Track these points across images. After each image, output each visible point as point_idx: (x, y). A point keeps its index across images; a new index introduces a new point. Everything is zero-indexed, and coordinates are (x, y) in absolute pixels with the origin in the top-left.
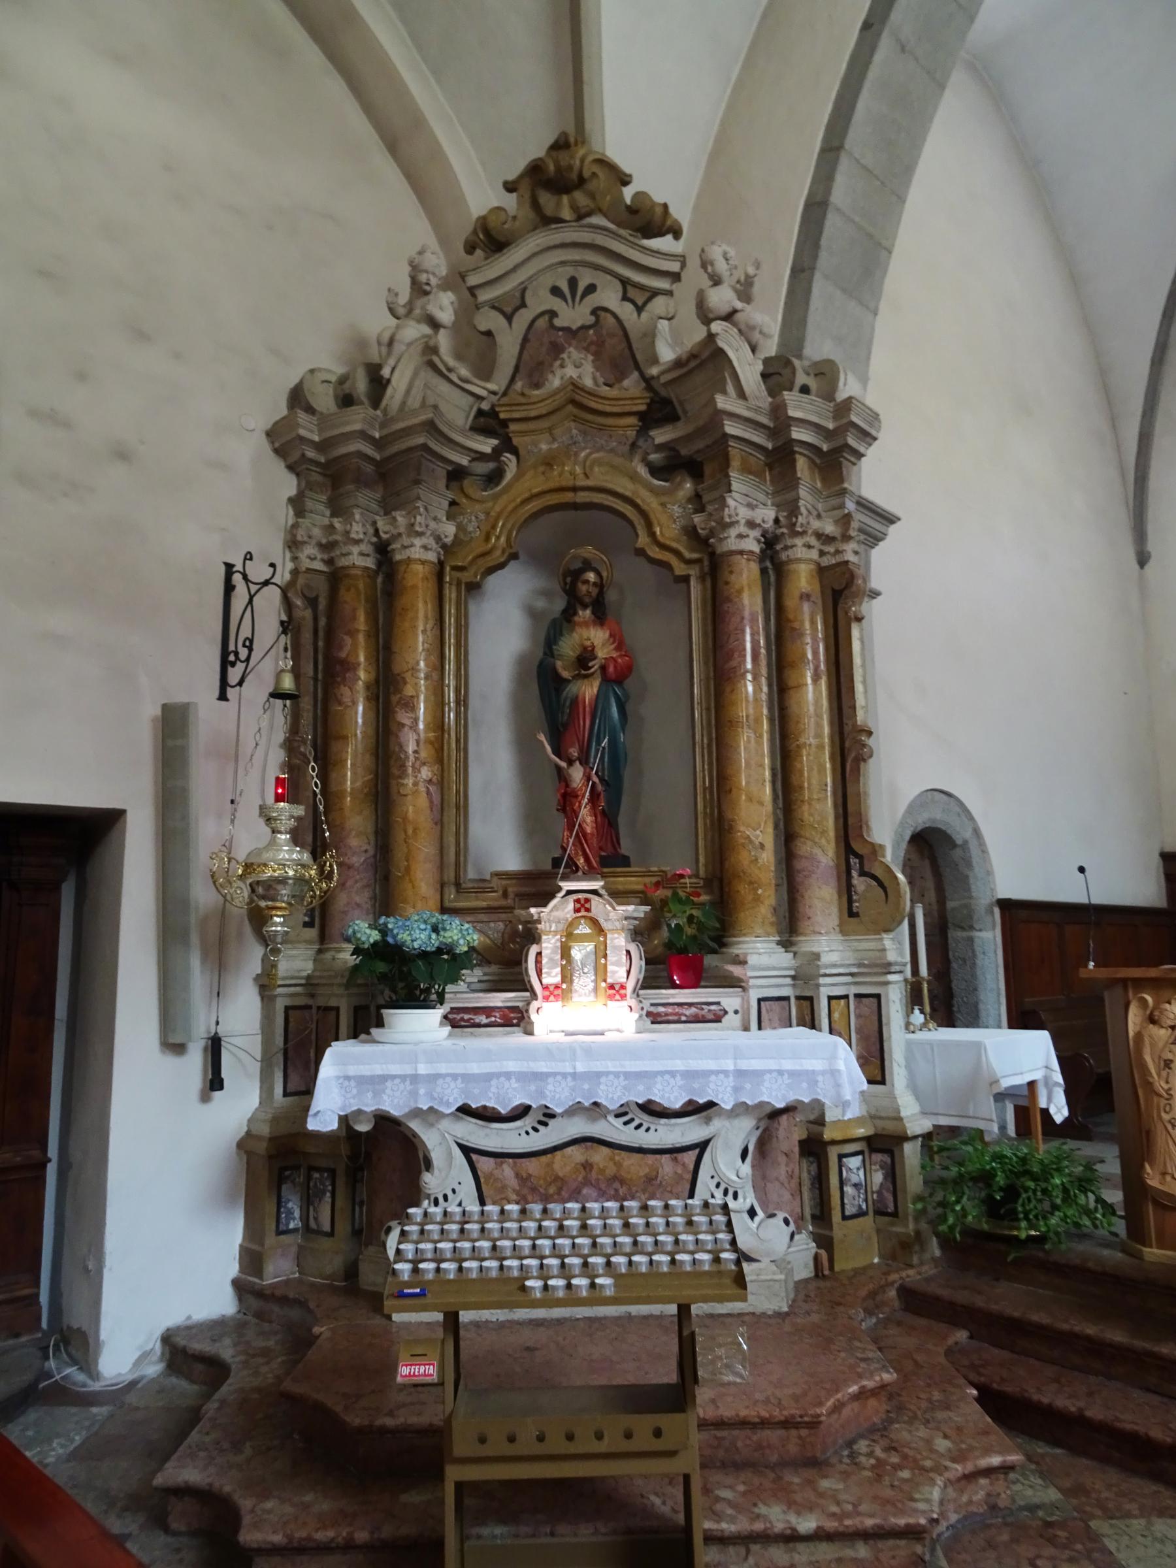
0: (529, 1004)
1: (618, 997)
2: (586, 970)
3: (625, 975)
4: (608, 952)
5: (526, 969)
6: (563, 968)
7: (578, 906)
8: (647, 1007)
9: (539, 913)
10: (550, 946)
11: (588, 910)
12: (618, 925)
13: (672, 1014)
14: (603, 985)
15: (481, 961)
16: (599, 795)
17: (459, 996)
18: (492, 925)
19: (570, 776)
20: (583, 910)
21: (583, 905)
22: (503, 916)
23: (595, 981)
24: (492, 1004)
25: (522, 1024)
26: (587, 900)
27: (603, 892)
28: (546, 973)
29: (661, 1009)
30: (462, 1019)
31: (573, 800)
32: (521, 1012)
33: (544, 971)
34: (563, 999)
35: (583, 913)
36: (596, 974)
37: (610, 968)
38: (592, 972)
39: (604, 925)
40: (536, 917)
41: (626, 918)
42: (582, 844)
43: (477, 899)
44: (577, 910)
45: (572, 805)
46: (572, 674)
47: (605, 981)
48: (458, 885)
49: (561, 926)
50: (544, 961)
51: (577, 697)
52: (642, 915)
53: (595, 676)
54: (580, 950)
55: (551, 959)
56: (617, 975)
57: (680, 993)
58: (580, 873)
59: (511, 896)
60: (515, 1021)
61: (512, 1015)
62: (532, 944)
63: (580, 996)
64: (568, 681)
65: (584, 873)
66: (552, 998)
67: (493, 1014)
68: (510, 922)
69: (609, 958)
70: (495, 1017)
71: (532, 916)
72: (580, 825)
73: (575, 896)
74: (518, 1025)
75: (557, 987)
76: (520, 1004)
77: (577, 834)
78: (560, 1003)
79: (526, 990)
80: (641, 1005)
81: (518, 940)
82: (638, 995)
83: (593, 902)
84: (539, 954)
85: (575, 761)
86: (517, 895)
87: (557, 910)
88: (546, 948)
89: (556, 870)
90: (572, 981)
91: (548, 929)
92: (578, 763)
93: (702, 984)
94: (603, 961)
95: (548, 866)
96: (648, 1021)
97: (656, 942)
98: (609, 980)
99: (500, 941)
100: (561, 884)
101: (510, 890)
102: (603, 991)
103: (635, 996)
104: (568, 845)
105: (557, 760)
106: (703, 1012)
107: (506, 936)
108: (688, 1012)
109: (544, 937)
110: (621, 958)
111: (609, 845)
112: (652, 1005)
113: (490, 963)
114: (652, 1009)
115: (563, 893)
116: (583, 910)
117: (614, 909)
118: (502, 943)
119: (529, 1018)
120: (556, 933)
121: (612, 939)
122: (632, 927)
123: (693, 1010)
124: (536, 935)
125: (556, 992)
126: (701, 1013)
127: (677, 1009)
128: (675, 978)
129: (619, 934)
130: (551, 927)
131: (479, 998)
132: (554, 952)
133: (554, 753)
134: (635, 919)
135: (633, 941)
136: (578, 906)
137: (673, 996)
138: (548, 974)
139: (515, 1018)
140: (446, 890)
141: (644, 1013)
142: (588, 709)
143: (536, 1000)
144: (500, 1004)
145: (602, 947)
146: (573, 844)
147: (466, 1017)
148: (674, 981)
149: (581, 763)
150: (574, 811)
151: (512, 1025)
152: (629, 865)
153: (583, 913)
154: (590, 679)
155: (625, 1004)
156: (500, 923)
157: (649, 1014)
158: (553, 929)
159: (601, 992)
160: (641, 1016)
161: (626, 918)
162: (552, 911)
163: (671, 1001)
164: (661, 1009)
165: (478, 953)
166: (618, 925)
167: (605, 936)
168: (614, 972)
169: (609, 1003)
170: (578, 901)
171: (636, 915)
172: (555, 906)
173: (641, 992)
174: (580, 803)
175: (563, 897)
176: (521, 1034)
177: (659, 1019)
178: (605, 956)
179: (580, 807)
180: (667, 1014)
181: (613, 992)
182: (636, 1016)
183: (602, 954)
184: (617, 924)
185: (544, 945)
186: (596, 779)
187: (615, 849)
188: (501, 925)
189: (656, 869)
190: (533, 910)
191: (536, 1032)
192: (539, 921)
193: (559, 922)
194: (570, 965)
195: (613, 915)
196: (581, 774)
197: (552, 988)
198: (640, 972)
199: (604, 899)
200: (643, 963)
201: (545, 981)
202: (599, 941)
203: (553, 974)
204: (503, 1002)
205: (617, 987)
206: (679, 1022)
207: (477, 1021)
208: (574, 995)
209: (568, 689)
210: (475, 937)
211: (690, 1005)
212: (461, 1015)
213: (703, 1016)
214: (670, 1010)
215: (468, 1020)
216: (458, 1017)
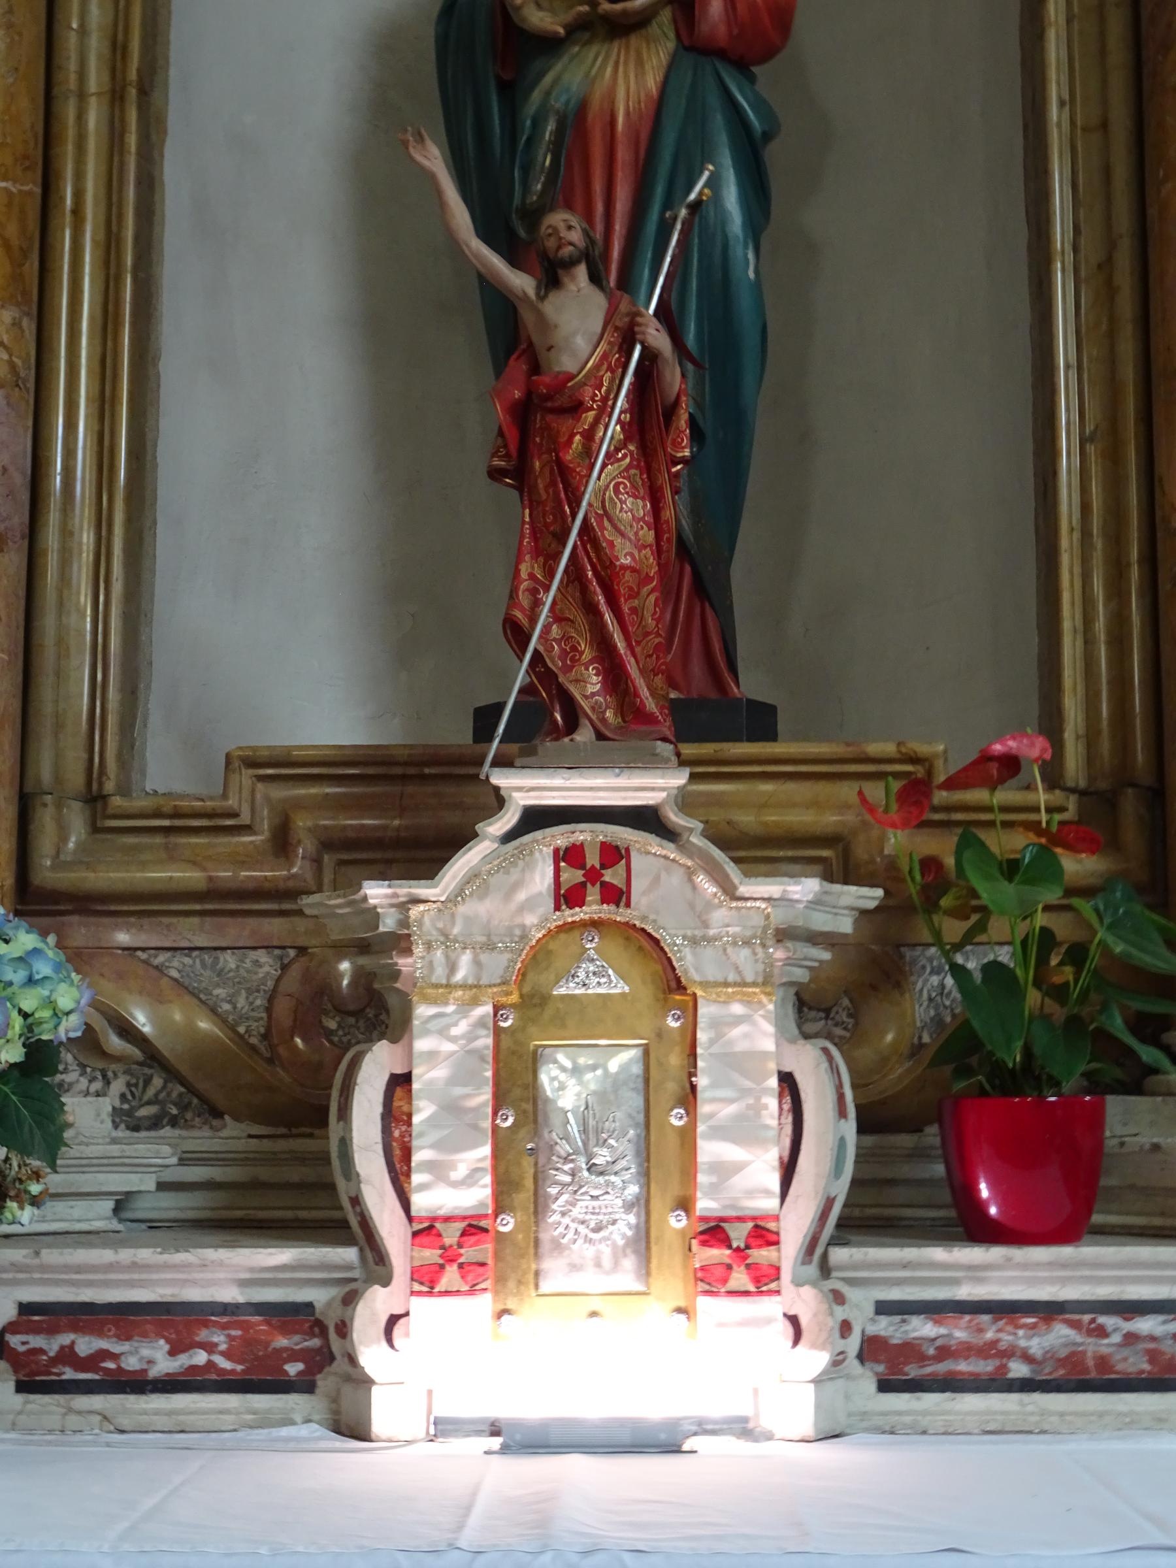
0: (350, 1299)
1: (740, 1278)
2: (602, 1157)
3: (774, 1181)
4: (701, 1081)
5: (345, 1144)
6: (502, 1146)
7: (572, 876)
8: (865, 1322)
9: (403, 907)
10: (448, 1047)
11: (616, 895)
12: (746, 962)
13: (966, 1351)
14: (678, 1222)
15: (184, 1107)
16: (671, 412)
17: (52, 1256)
18: (229, 960)
19: (544, 324)
20: (593, 893)
21: (593, 876)
22: (275, 927)
23: (643, 1204)
24: (194, 1294)
25: (325, 1382)
26: (613, 854)
27: (675, 818)
28: (430, 1166)
29: (923, 1328)
30: (67, 1356)
31: (563, 425)
32: (319, 1327)
33: (419, 1157)
34: (500, 1280)
35: (592, 909)
36: (645, 1175)
37: (709, 1150)
38: (630, 1165)
39: (688, 962)
40: (388, 924)
41: (783, 935)
42: (591, 610)
43: (172, 857)
44: (568, 897)
45: (557, 446)
46: (569, 16)
47: (685, 1204)
48: (94, 800)
49: (497, 964)
50: (423, 1112)
51: (583, 107)
52: (845, 925)
53: (654, 29)
54: (576, 1071)
55: (451, 1108)
56: (739, 1182)
57: (1008, 1263)
58: (585, 735)
59: (305, 847)
60: (293, 1369)
61: (282, 1342)
62: (371, 1041)
63: (574, 1267)
64: (550, 46)
65: (600, 736)
66: (451, 1277)
67: (203, 1335)
68: (302, 950)
69: (704, 1109)
70: (210, 1348)
71: (373, 916)
72: (586, 527)
73: (561, 836)
74: (305, 1385)
75: (473, 1228)
76: (318, 1296)
77: (575, 572)
78: (484, 1303)
79: (350, 1241)
80: (841, 1313)
81: (332, 1024)
82: (825, 1270)
83: (636, 861)
84: (400, 1082)
85: (570, 263)
86: (328, 843)
87: (483, 892)
88: (432, 1056)
89: (479, 748)
90: (539, 1207)
91: (439, 975)
92: (581, 272)
93: (1097, 1218)
94: (677, 1118)
95: (459, 734)
96: (865, 1381)
97: (889, 1037)
98: (705, 1205)
99: (259, 1027)
100: (502, 779)
101: (302, 822)
102: (677, 1245)
103: (812, 1270)
104: (533, 620)
105: (497, 262)
106: (1104, 1346)
107: (283, 1007)
108: (1036, 1345)
109: (422, 1011)
110: (758, 1108)
111: (697, 668)
112: (883, 1308)
113: (217, 1113)
114: (884, 1326)
115: (507, 820)
116: (593, 893)
117: (730, 892)
118: (265, 1037)
119: (352, 1360)
120: (474, 991)
121: (718, 1025)
122: (801, 975)
123: (1060, 1335)
124: (392, 1001)
125: (468, 1254)
126: (1093, 1347)
127: (992, 1331)
128: (984, 1191)
129: (748, 1001)
130: (452, 968)
131: (134, 1266)
132: (462, 1076)
133: (486, 233)
134: (814, 938)
135: (806, 1036)
136: (572, 876)
137: (974, 1271)
138: (437, 1169)
139: (294, 1356)
140: (45, 819)
141: (853, 1344)
142: (623, 154)
143: (386, 1282)
144: (230, 1294)
145: (675, 1059)
146: (557, 616)
147: (85, 1345)
148: (980, 1207)
149: (596, 279)
150: (563, 471)
151: (282, 1386)
152: (770, 735)
153: (592, 909)
154: (634, 40)
155: (771, 1308)
156: (262, 956)
157: (872, 1349)
158: (459, 976)
159: (668, 1255)
160: (837, 1362)
161: (783, 935)
162: (458, 896)
163: (965, 1292)
164: (923, 1328)
165: (171, 1073)
166: (746, 962)
167: (691, 1013)
168: (725, 1170)
169: (703, 1302)
170: (571, 855)
171: (822, 922)
172: (473, 876)
173: (839, 1255)
174: (589, 436)
175: (509, 837)
176: (316, 1430)
177: (913, 1371)
178: (689, 1097)
179: (589, 453)
180: (945, 1352)
181: (717, 1254)
182: (820, 1360)
183: (672, 1087)
184: (742, 956)
185: (421, 1045)
186: (658, 338)
187: (722, 688)
188: (266, 965)
189: (890, 749)
190: (376, 892)
191: (379, 1424)
192: (401, 942)
193: (490, 946)
194: (536, 1133)
195: (722, 919)
196: (596, 322)
197: (451, 1234)
198: (838, 1171)
199: (685, 848)
200: (849, 1128)
201: (422, 1202)
202: (661, 1033)
203: (460, 1172)
204: (243, 1284)
205: (738, 1234)
206: (999, 1384)
207: (132, 1363)
208: (547, 1264)
209: (548, 79)
210: (66, 997)
211: (1050, 1311)
212: (65, 1339)
213: (1103, 1362)
214: (959, 1332)
215: (92, 1362)
216: (52, 1345)
